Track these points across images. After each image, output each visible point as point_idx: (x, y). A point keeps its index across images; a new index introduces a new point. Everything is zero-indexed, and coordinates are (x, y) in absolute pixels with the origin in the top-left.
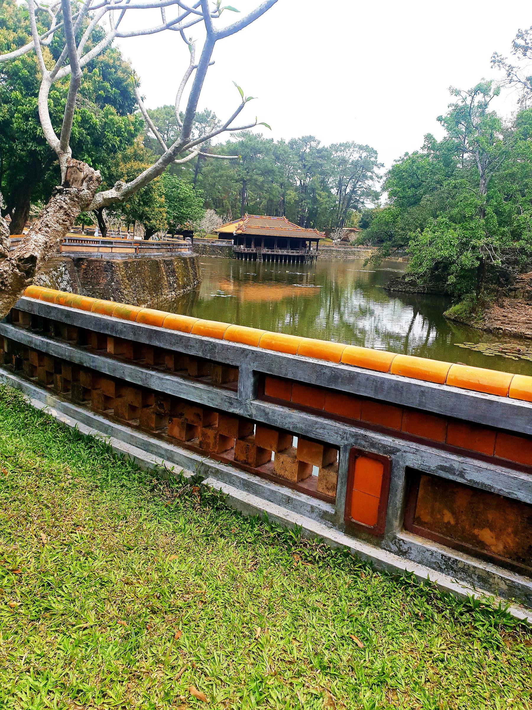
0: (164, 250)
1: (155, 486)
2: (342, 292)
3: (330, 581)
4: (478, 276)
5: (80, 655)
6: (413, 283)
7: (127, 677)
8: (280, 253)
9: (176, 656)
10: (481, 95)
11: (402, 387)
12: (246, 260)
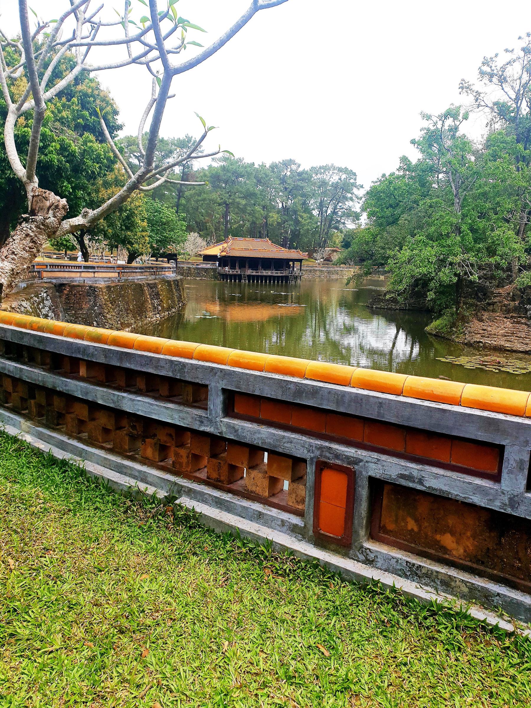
0: (148, 273)
1: (129, 508)
2: (327, 309)
3: (300, 593)
4: (457, 291)
5: (44, 678)
6: (394, 300)
7: (91, 698)
8: (265, 274)
9: (142, 675)
10: (451, 119)
11: (361, 400)
12: (231, 281)
